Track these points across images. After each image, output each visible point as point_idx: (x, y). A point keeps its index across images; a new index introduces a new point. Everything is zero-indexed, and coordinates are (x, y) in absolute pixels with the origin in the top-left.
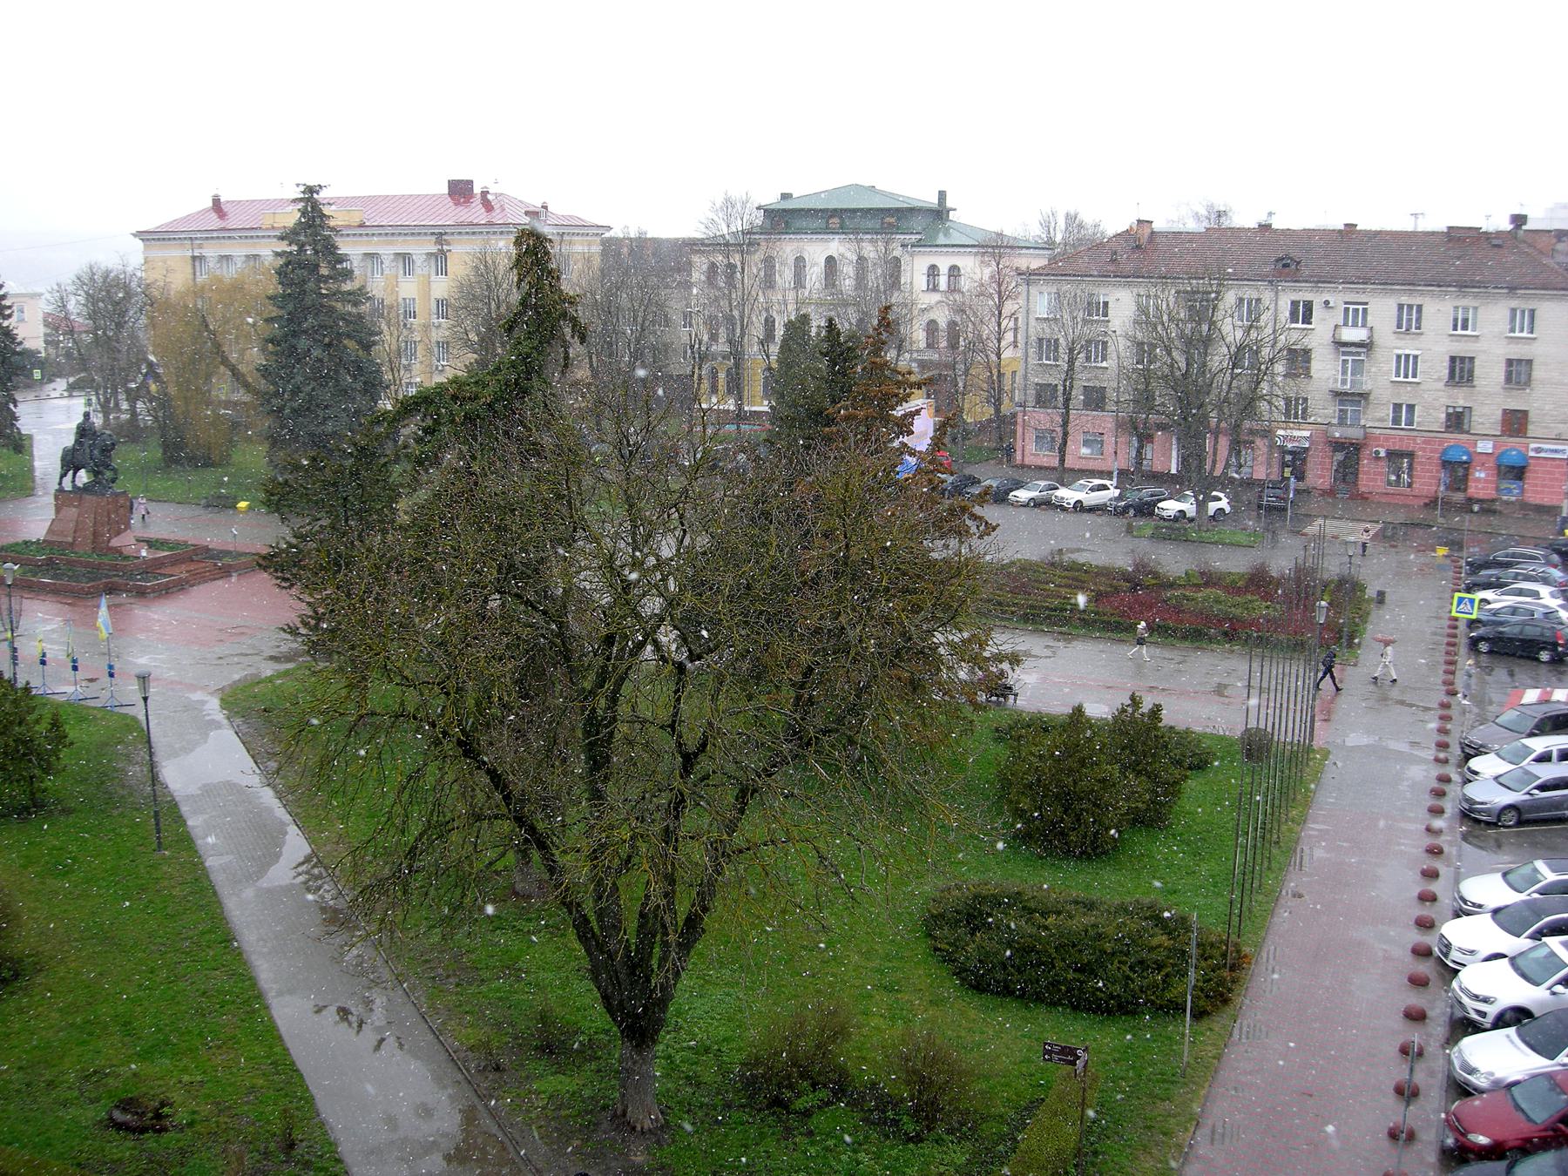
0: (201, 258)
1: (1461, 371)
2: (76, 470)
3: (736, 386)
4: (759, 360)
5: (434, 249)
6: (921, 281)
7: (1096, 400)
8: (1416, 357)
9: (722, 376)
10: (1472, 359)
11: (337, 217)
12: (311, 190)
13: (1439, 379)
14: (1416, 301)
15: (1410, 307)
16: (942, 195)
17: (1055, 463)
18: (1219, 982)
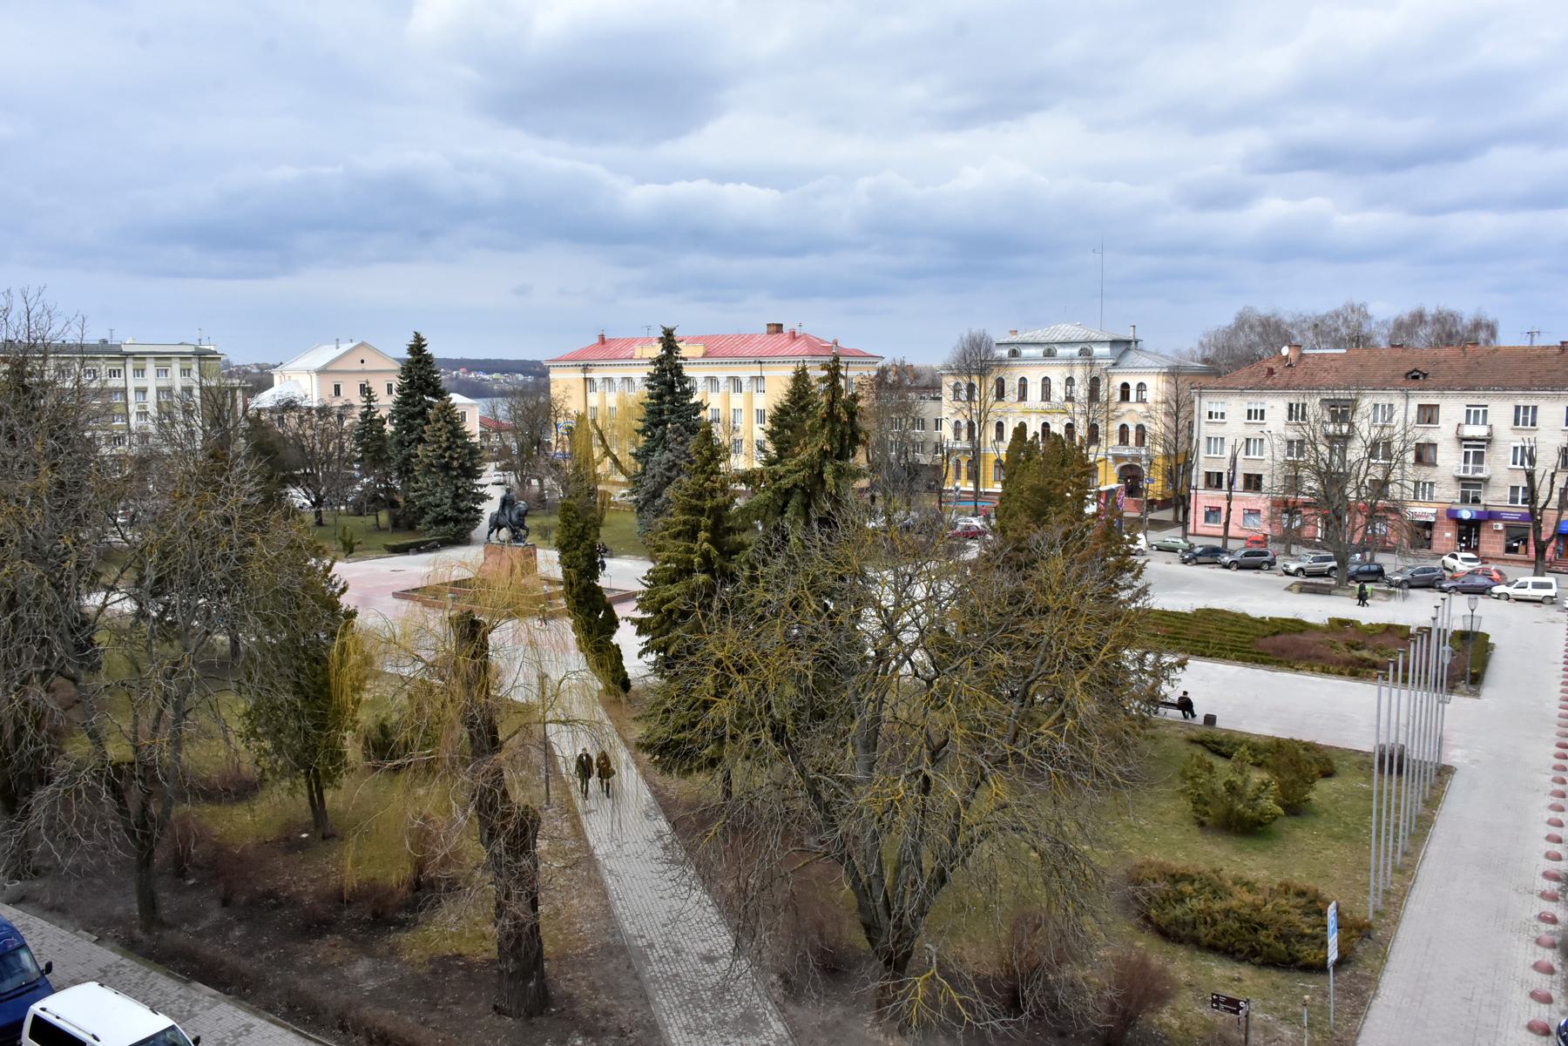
2: (500, 528)
3: (974, 476)
4: (996, 450)
7: (1253, 482)
9: (964, 464)
14: (1531, 402)
15: (1526, 408)
17: (1221, 532)
18: (1366, 938)
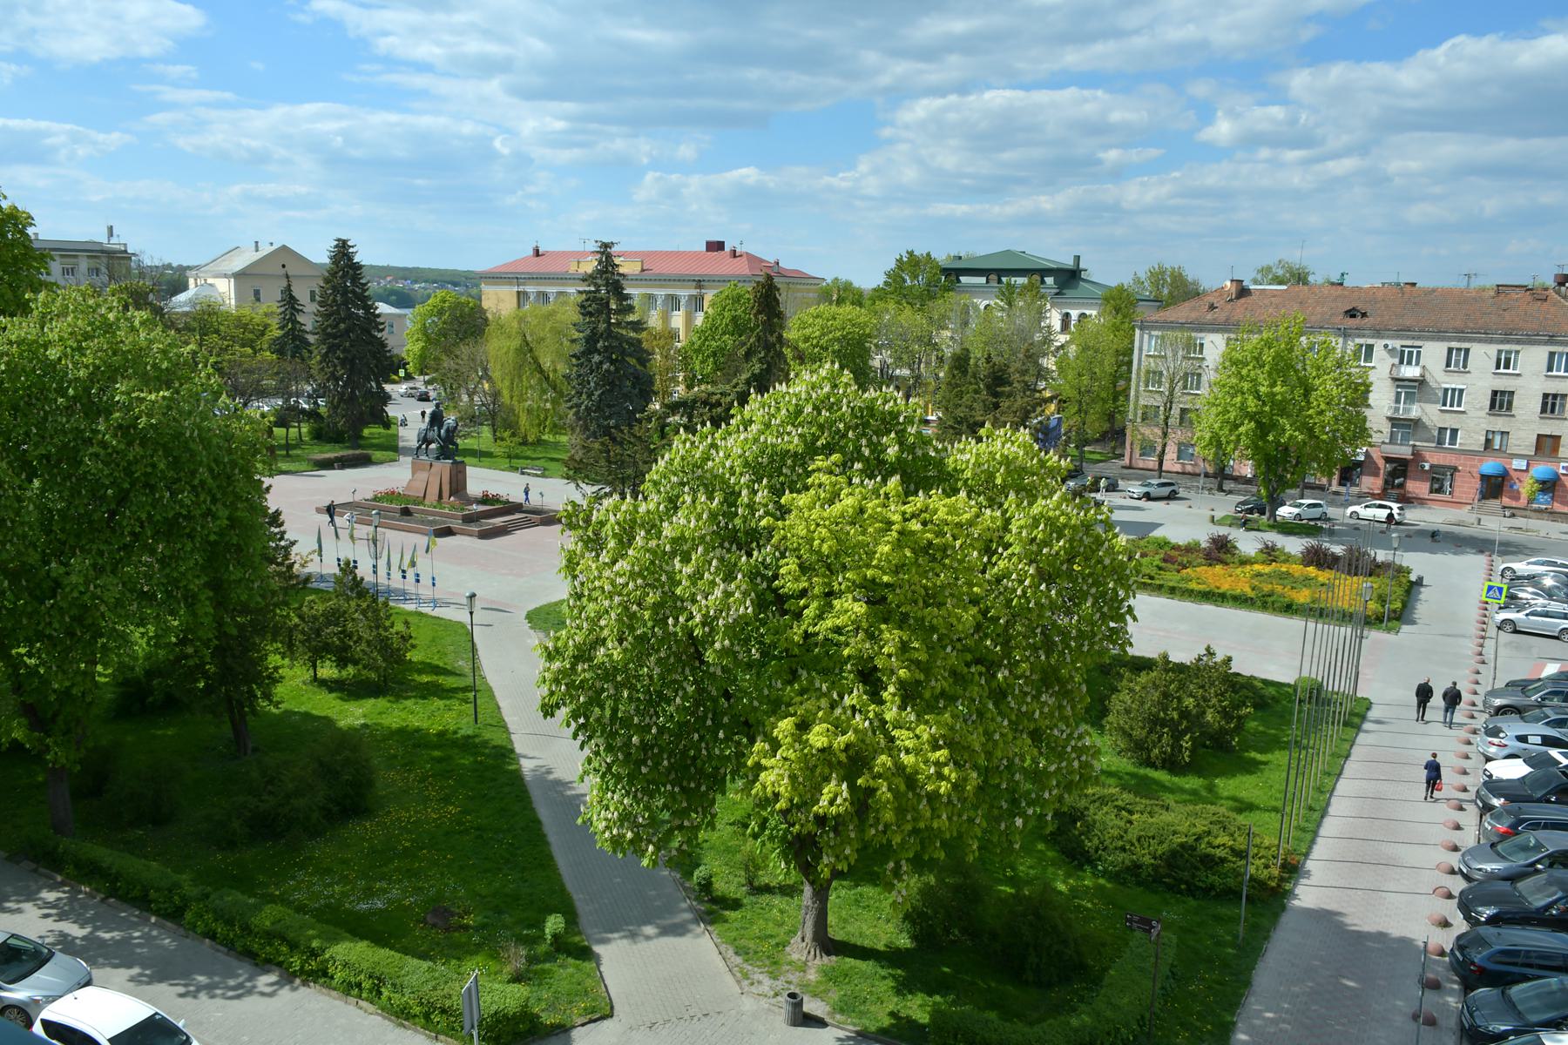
0: (525, 293)
1: (1500, 402)
5: (694, 292)
6: (1056, 323)
8: (1461, 391)
10: (1512, 393)
11: (627, 267)
12: (606, 246)
13: (1481, 409)
15: (1459, 350)
16: (1077, 258)
